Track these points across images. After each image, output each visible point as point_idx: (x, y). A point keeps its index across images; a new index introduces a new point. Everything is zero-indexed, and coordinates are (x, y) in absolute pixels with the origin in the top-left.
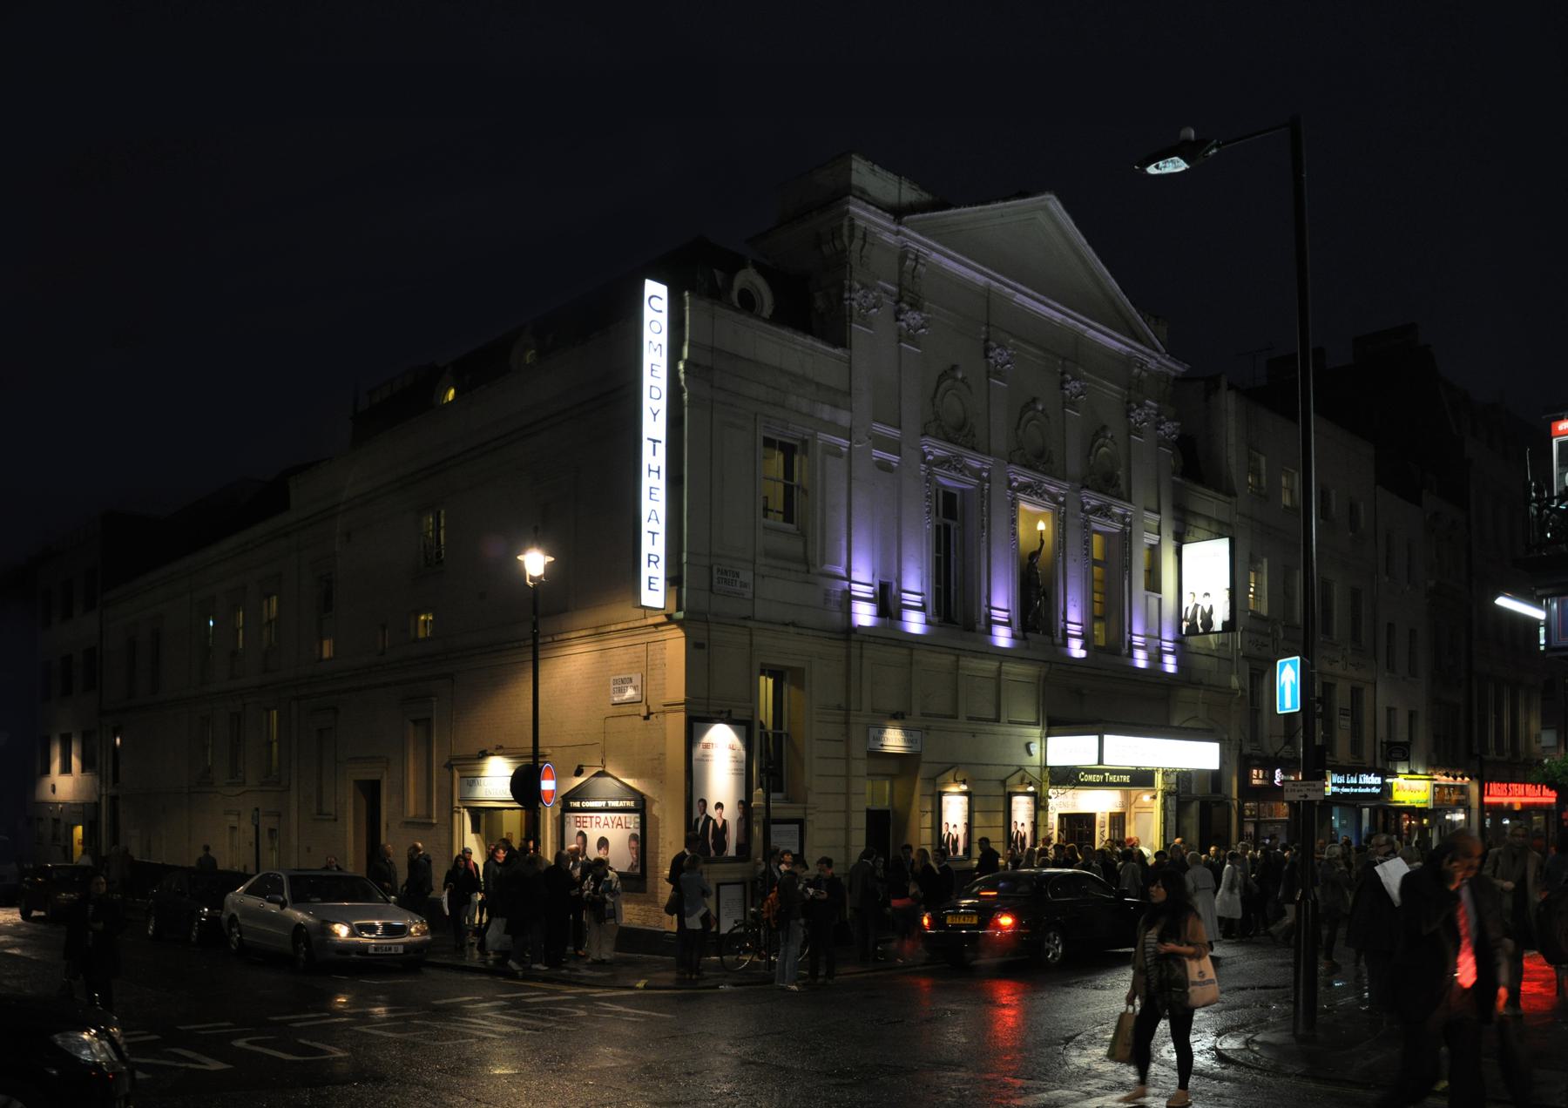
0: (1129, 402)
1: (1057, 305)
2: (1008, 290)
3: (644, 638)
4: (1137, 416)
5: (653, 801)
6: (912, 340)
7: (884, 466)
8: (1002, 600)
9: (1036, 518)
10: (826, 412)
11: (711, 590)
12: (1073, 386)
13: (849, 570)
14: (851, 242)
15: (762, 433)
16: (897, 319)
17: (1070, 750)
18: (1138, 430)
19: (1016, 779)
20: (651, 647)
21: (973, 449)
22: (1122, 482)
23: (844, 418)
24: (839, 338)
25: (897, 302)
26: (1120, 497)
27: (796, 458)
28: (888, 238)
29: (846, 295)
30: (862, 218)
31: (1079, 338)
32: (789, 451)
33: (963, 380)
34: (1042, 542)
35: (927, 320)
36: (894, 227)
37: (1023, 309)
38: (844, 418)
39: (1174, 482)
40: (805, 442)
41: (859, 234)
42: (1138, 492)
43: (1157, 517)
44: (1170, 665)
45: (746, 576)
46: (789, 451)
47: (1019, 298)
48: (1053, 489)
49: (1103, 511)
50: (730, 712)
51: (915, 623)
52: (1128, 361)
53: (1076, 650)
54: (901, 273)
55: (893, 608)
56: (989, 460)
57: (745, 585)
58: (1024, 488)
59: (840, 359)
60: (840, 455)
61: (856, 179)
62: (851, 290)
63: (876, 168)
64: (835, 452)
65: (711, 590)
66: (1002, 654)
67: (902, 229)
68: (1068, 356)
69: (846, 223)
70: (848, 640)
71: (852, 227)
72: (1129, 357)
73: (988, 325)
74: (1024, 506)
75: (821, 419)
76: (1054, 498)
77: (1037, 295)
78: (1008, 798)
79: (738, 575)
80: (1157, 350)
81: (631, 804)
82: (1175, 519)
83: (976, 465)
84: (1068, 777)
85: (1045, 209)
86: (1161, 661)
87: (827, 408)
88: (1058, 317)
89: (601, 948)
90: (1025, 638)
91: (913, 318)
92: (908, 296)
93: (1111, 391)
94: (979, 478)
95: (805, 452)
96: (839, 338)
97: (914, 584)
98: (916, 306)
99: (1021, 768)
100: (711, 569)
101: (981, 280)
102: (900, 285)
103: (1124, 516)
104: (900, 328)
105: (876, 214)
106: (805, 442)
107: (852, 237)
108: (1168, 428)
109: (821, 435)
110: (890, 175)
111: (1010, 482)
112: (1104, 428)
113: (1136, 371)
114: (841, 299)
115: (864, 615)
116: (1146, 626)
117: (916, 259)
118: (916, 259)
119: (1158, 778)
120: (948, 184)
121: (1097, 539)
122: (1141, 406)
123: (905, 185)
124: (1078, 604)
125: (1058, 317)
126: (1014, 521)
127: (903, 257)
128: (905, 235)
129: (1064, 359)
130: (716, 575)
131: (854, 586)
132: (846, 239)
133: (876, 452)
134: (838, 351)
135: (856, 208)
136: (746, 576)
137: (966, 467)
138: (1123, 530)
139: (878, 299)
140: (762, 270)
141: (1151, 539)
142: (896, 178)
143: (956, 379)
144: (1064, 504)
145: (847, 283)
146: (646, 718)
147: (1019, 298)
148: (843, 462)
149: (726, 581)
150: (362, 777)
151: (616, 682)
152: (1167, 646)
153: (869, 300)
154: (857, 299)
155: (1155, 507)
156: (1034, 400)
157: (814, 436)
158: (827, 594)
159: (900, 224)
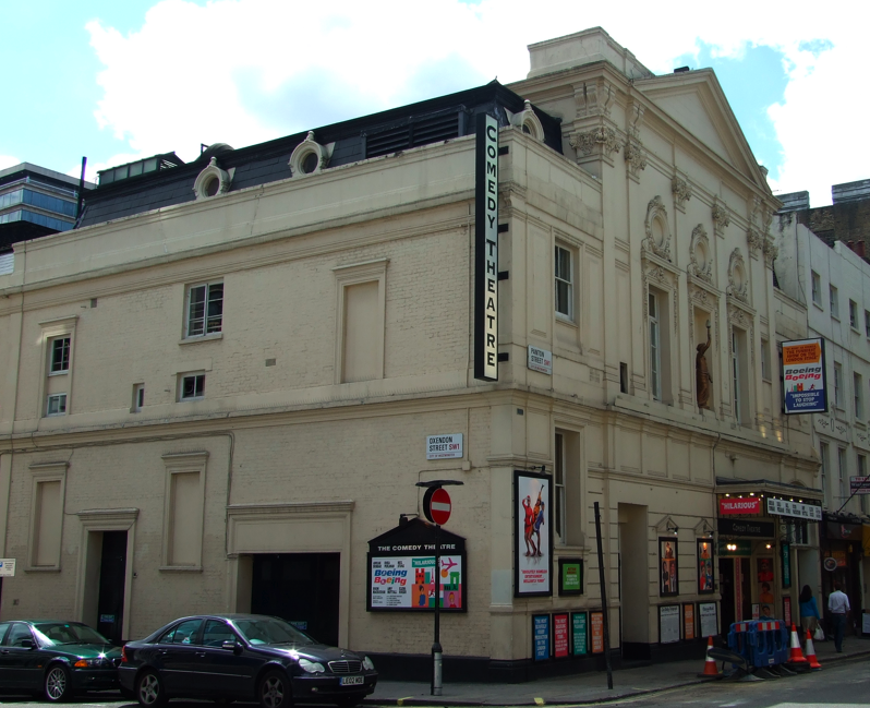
3: (468, 404)
24: (835, 362)
57: (547, 363)
100: (527, 348)
130: (531, 354)
149: (537, 360)
151: (433, 441)
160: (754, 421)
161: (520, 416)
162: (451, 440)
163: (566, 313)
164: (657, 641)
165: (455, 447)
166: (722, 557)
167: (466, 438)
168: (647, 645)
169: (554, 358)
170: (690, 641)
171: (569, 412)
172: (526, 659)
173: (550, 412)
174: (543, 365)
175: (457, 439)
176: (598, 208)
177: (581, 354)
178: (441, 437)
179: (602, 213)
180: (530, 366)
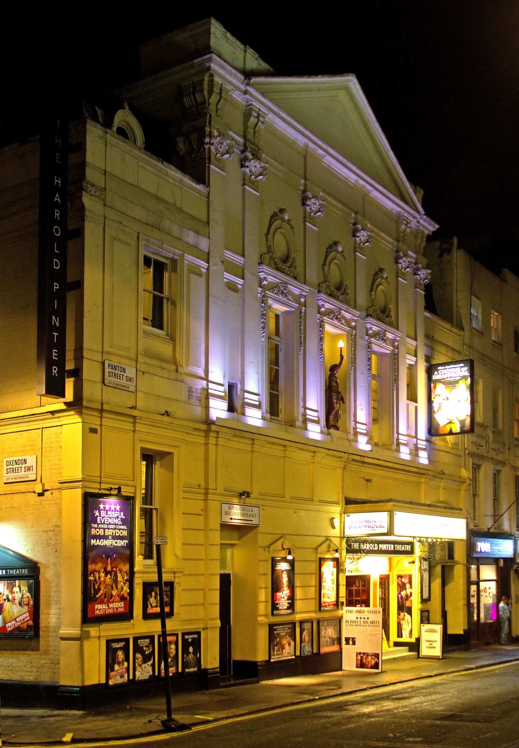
0: (397, 252)
1: (354, 168)
2: (320, 152)
3: (40, 424)
4: (403, 263)
5: (47, 567)
6: (255, 185)
7: (232, 287)
8: (314, 401)
9: (335, 338)
10: (190, 237)
11: (103, 382)
12: (363, 235)
13: (207, 372)
14: (210, 96)
15: (143, 252)
16: (242, 166)
17: (360, 524)
18: (402, 274)
19: (325, 547)
20: (45, 431)
21: (295, 278)
22: (393, 314)
23: (204, 244)
24: (201, 177)
25: (243, 152)
26: (391, 324)
27: (166, 275)
28: (238, 97)
29: (207, 140)
30: (220, 76)
31: (365, 197)
32: (159, 269)
33: (289, 220)
34: (342, 357)
35: (265, 169)
36: (242, 87)
37: (328, 170)
38: (204, 244)
39: (426, 317)
40: (174, 261)
41: (216, 90)
42: (403, 322)
43: (414, 343)
44: (423, 458)
45: (130, 372)
46: (159, 269)
47: (328, 160)
48: (348, 316)
49: (380, 336)
50: (119, 489)
51: (254, 418)
52: (398, 219)
53: (363, 444)
54: (246, 127)
55: (238, 405)
56: (306, 288)
57: (130, 379)
58: (328, 313)
59: (198, 192)
60: (200, 275)
61: (213, 42)
62: (211, 136)
63: (228, 35)
64: (195, 271)
65: (103, 382)
66: (314, 445)
67: (250, 89)
68: (358, 212)
69: (206, 79)
70: (207, 432)
71: (211, 82)
72: (399, 216)
73: (305, 179)
74: (328, 328)
75: (187, 243)
76: (348, 322)
77: (341, 158)
78: (321, 561)
79: (124, 370)
80: (419, 213)
81: (25, 572)
82: (427, 345)
83: (297, 292)
84: (354, 547)
85: (347, 89)
86: (417, 455)
87: (192, 234)
88: (353, 178)
89: (419, 551)
90: (329, 434)
91: (254, 166)
92: (250, 149)
93: (387, 242)
94: (300, 303)
95: (174, 269)
96: (201, 177)
97: (254, 384)
98: (256, 156)
99: (327, 539)
100: (103, 363)
101: (301, 141)
102: (245, 137)
103: (394, 341)
104: (244, 174)
105: (230, 73)
106: (174, 261)
107: (211, 91)
108: (423, 274)
109: (188, 257)
110: (238, 43)
111: (319, 307)
112: (381, 270)
113: (403, 227)
114: (202, 143)
115: (218, 410)
116: (408, 428)
117: (258, 117)
118: (258, 117)
119: (418, 547)
120: (288, 54)
121: (374, 358)
122: (406, 255)
123: (250, 52)
124: (364, 408)
125: (353, 178)
126: (321, 339)
127: (247, 115)
128: (251, 95)
129: (356, 213)
130: (107, 370)
131: (211, 385)
132: (206, 93)
133: (227, 275)
134: (200, 187)
135: (216, 66)
136: (130, 372)
137: (290, 292)
138: (393, 351)
139: (230, 146)
140: (135, 112)
141: (410, 360)
142: (242, 46)
143: (283, 220)
144: (355, 328)
145: (207, 129)
146: (41, 495)
147: (328, 160)
148: (203, 279)
149: (115, 376)
150: (142, 446)
151: (9, 463)
152: (422, 444)
153: (222, 145)
154: (216, 145)
155: (412, 334)
156: (336, 243)
157: (182, 256)
158: (190, 391)
159: (248, 84)
160: (301, 419)
161: (93, 435)
162: (25, 461)
163: (161, 328)
164: (495, 582)
165: (29, 469)
166: (453, 561)
167: (39, 460)
168: (255, 663)
169: (140, 374)
170: (308, 657)
171: (154, 430)
172: (99, 685)
173: (285, 457)
174: (124, 382)
175: (31, 461)
176: (205, 220)
177: (177, 371)
178: (16, 458)
179: (208, 223)
180: (106, 382)
